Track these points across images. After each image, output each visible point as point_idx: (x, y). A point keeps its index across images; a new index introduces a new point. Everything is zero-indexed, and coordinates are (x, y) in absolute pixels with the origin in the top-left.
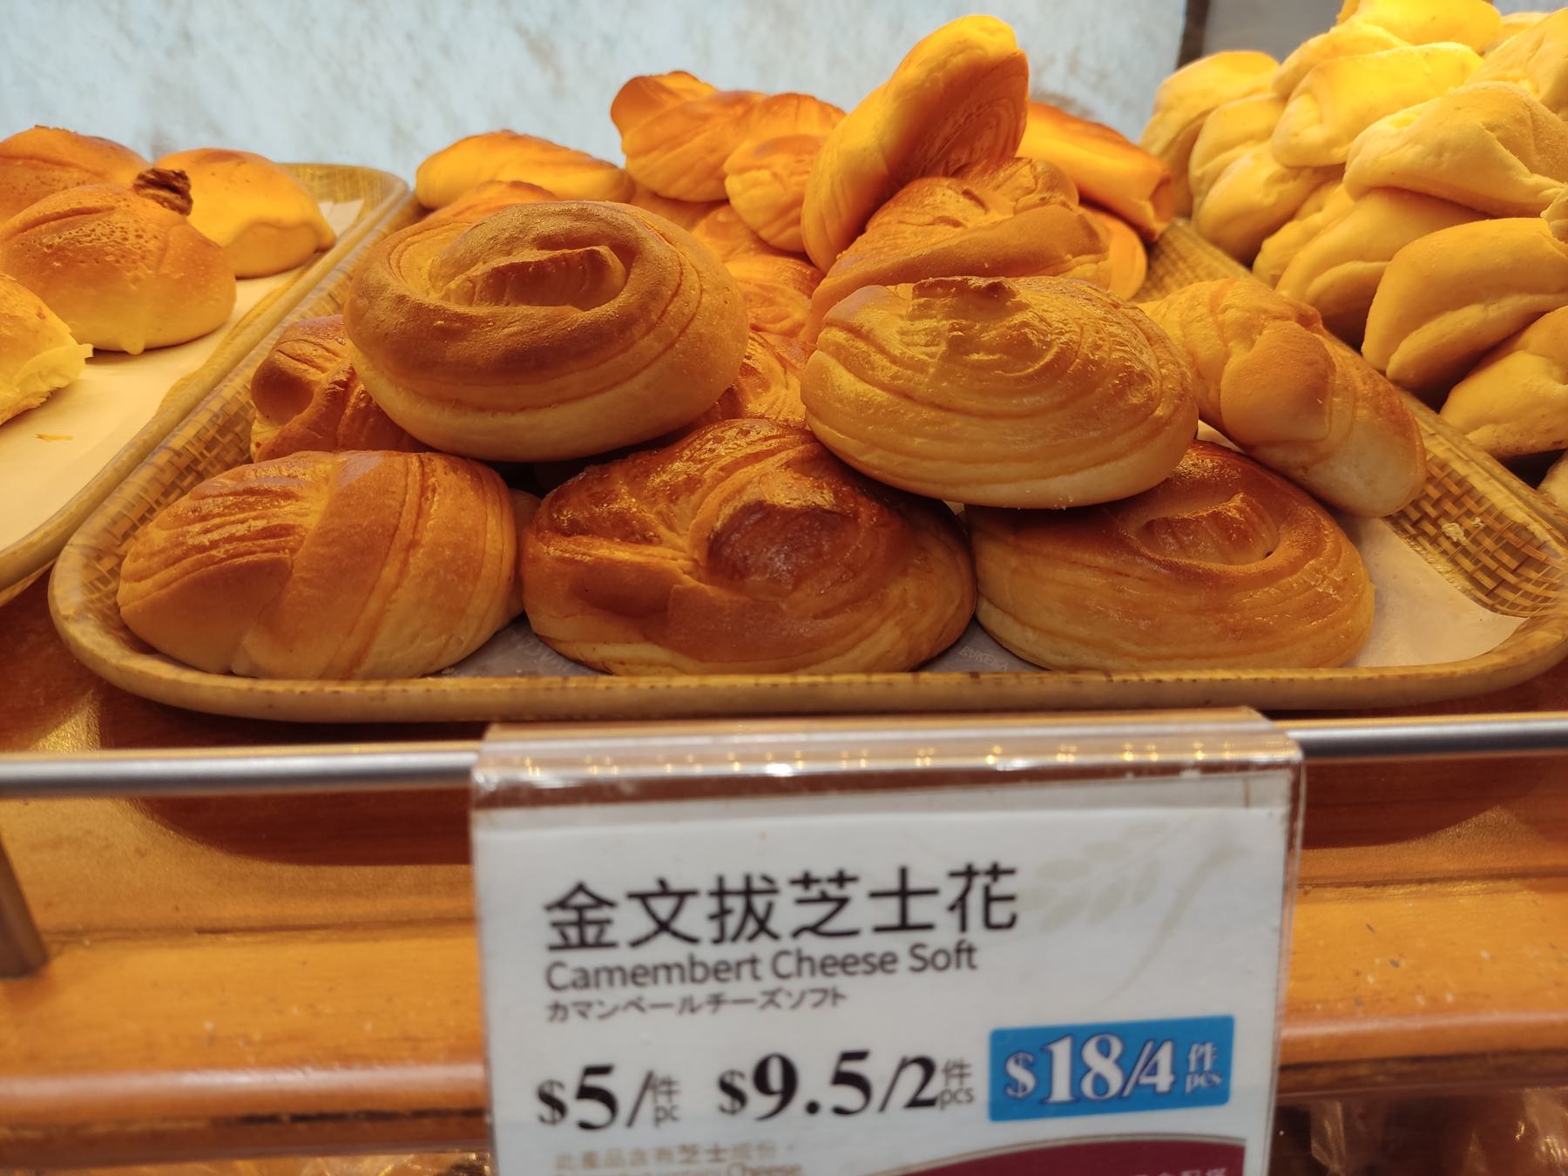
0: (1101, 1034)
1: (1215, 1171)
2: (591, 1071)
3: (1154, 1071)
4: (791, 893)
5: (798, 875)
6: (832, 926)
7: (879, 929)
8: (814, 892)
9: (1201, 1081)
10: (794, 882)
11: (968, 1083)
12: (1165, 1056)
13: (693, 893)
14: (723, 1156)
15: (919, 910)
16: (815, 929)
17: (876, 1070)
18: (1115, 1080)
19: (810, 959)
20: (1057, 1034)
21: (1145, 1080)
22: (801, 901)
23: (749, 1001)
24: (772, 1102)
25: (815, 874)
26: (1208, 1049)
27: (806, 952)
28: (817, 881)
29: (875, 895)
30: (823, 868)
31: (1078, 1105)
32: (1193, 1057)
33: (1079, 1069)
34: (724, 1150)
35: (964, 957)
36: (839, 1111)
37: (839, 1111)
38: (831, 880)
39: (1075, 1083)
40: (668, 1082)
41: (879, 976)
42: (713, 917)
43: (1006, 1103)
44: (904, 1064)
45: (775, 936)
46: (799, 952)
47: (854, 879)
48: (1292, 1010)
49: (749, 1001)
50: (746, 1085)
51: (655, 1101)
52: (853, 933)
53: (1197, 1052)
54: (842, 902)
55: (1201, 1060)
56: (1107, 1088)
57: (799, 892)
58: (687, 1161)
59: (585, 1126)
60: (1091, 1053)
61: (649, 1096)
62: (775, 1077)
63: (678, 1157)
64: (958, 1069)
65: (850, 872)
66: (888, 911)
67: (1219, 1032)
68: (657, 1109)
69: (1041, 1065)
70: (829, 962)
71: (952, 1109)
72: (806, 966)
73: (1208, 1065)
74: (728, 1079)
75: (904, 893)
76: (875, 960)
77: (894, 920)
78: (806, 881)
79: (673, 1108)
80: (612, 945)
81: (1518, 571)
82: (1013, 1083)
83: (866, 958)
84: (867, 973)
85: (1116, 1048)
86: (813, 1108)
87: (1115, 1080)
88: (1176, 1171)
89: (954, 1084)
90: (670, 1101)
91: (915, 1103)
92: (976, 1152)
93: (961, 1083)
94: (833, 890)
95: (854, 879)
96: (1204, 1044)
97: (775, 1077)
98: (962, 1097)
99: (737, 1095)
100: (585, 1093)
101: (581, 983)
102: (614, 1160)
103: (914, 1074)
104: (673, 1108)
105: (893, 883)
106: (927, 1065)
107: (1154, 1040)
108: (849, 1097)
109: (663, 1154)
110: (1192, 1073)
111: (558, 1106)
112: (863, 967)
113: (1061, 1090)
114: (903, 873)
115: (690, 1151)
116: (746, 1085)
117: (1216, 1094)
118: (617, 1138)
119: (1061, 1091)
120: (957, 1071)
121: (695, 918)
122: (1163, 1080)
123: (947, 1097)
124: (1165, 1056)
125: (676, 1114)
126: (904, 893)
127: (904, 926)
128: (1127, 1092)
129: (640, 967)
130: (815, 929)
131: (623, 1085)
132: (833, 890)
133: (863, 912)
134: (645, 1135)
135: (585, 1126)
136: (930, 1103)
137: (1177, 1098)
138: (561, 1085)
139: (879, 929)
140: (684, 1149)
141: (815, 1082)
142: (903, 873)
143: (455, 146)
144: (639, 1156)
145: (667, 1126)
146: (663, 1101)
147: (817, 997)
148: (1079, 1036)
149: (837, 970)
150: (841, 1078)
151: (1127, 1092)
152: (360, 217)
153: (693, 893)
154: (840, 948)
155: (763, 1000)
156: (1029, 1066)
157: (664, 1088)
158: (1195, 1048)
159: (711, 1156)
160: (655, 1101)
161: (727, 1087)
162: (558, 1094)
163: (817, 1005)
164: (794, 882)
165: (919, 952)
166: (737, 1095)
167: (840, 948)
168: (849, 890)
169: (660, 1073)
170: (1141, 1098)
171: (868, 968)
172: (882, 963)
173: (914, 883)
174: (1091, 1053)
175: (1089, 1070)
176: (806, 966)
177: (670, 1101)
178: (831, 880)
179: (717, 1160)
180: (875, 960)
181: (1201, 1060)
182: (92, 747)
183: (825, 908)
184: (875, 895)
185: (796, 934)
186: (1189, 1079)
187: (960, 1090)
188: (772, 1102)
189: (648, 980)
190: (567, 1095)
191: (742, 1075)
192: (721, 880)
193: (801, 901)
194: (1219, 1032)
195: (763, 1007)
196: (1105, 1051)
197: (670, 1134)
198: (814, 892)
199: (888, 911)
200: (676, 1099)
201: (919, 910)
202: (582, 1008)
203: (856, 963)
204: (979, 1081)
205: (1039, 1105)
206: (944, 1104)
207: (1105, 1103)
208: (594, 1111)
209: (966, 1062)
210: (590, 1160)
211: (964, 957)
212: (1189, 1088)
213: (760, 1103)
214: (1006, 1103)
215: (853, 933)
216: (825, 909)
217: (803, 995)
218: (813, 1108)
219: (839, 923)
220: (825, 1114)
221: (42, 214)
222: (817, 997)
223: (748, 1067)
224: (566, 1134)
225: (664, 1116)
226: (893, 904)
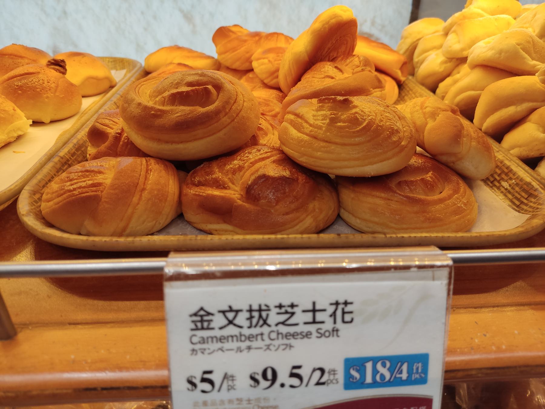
0: (383, 360)
1: (422, 407)
2: (205, 372)
3: (401, 373)
4: (275, 311)
5: (277, 304)
6: (289, 322)
7: (306, 323)
8: (283, 310)
9: (417, 376)
10: (276, 307)
11: (337, 377)
12: (405, 367)
13: (241, 311)
14: (251, 402)
15: (319, 316)
16: (283, 323)
17: (304, 372)
18: (388, 376)
19: (282, 334)
20: (368, 359)
21: (398, 376)
22: (278, 314)
23: (260, 348)
24: (268, 383)
25: (283, 304)
26: (420, 365)
27: (280, 331)
28: (284, 306)
29: (304, 311)
30: (286, 302)
31: (375, 384)
32: (415, 368)
33: (375, 372)
34: (252, 400)
35: (335, 333)
36: (292, 386)
37: (292, 386)
38: (289, 306)
39: (374, 376)
40: (232, 376)
41: (306, 340)
42: (248, 319)
43: (350, 384)
44: (314, 370)
45: (269, 326)
46: (278, 331)
47: (297, 306)
48: (449, 351)
49: (260, 348)
50: (259, 377)
51: (228, 383)
52: (296, 325)
53: (416, 366)
54: (293, 314)
55: (417, 369)
56: (385, 378)
57: (278, 310)
58: (239, 404)
59: (203, 392)
60: (379, 366)
61: (225, 381)
62: (269, 375)
63: (236, 402)
64: (333, 372)
65: (295, 303)
66: (309, 317)
67: (424, 359)
68: (229, 386)
69: (362, 370)
70: (288, 334)
71: (331, 386)
72: (280, 336)
73: (420, 370)
74: (253, 375)
75: (314, 311)
76: (304, 334)
77: (311, 320)
78: (280, 306)
79: (234, 385)
80: (213, 329)
81: (528, 199)
82: (352, 377)
83: (301, 333)
84: (301, 338)
85: (388, 364)
86: (282, 385)
87: (388, 376)
88: (409, 407)
89: (332, 377)
90: (233, 383)
91: (318, 384)
92: (339, 401)
93: (334, 377)
94: (289, 310)
95: (297, 306)
96: (418, 363)
97: (269, 375)
98: (334, 381)
99: (256, 381)
100: (203, 380)
101: (202, 342)
102: (214, 403)
103: (318, 374)
104: (234, 385)
105: (310, 307)
106: (322, 371)
107: (401, 362)
108: (295, 381)
109: (230, 401)
110: (414, 373)
111: (194, 385)
112: (300, 336)
113: (369, 379)
114: (314, 304)
115: (240, 400)
116: (259, 377)
117: (423, 381)
118: (214, 396)
119: (369, 380)
120: (332, 373)
121: (242, 319)
122: (404, 376)
123: (329, 382)
124: (405, 367)
125: (235, 387)
126: (314, 311)
127: (314, 322)
128: (392, 380)
129: (222, 336)
130: (283, 323)
131: (216, 377)
132: (289, 310)
133: (300, 317)
134: (224, 395)
135: (203, 392)
136: (323, 384)
137: (409, 382)
138: (195, 377)
139: (306, 323)
140: (238, 399)
141: (283, 376)
142: (314, 304)
143: (158, 51)
144: (222, 402)
145: (232, 391)
146: (230, 383)
147: (284, 347)
148: (375, 360)
149: (291, 337)
150: (292, 375)
151: (392, 380)
152: (125, 75)
153: (241, 311)
154: (292, 330)
155: (265, 348)
156: (358, 371)
157: (231, 378)
158: (415, 364)
159: (247, 402)
160: (228, 383)
161: (253, 378)
162: (194, 380)
163: (284, 349)
164: (276, 307)
165: (320, 331)
166: (256, 381)
167: (292, 330)
168: (295, 310)
169: (230, 373)
170: (397, 382)
171: (302, 337)
172: (307, 335)
173: (318, 307)
174: (379, 366)
175: (378, 372)
176: (280, 336)
177: (233, 383)
178: (289, 306)
179: (249, 403)
180: (304, 334)
181: (417, 369)
182: (32, 260)
183: (287, 316)
184: (304, 311)
185: (277, 325)
186: (413, 375)
187: (334, 379)
188: (268, 383)
189: (225, 341)
190: (197, 381)
191: (258, 374)
192: (251, 306)
193: (278, 314)
194: (424, 359)
195: (265, 350)
196: (384, 365)
197: (233, 395)
198: (283, 310)
199: (309, 317)
200: (235, 382)
201: (319, 316)
202: (202, 351)
203: (298, 335)
204: (340, 376)
205: (361, 384)
206: (328, 384)
207: (384, 383)
208: (207, 386)
209: (336, 369)
210: (205, 403)
211: (335, 333)
212: (413, 378)
213: (264, 384)
214: (350, 384)
215: (296, 325)
216: (287, 316)
217: (279, 346)
218: (282, 385)
219: (292, 321)
220: (287, 388)
221: (14, 75)
222: (284, 347)
223: (260, 371)
224: (197, 394)
225: (231, 388)
226: (310, 315)
